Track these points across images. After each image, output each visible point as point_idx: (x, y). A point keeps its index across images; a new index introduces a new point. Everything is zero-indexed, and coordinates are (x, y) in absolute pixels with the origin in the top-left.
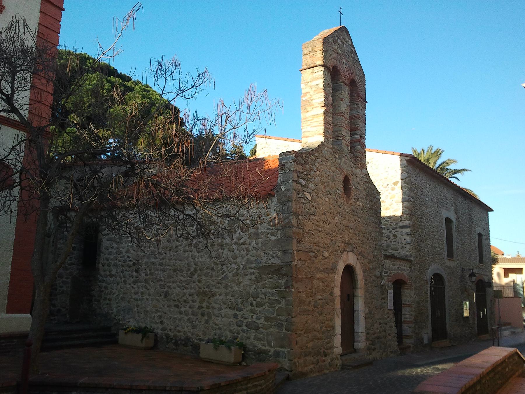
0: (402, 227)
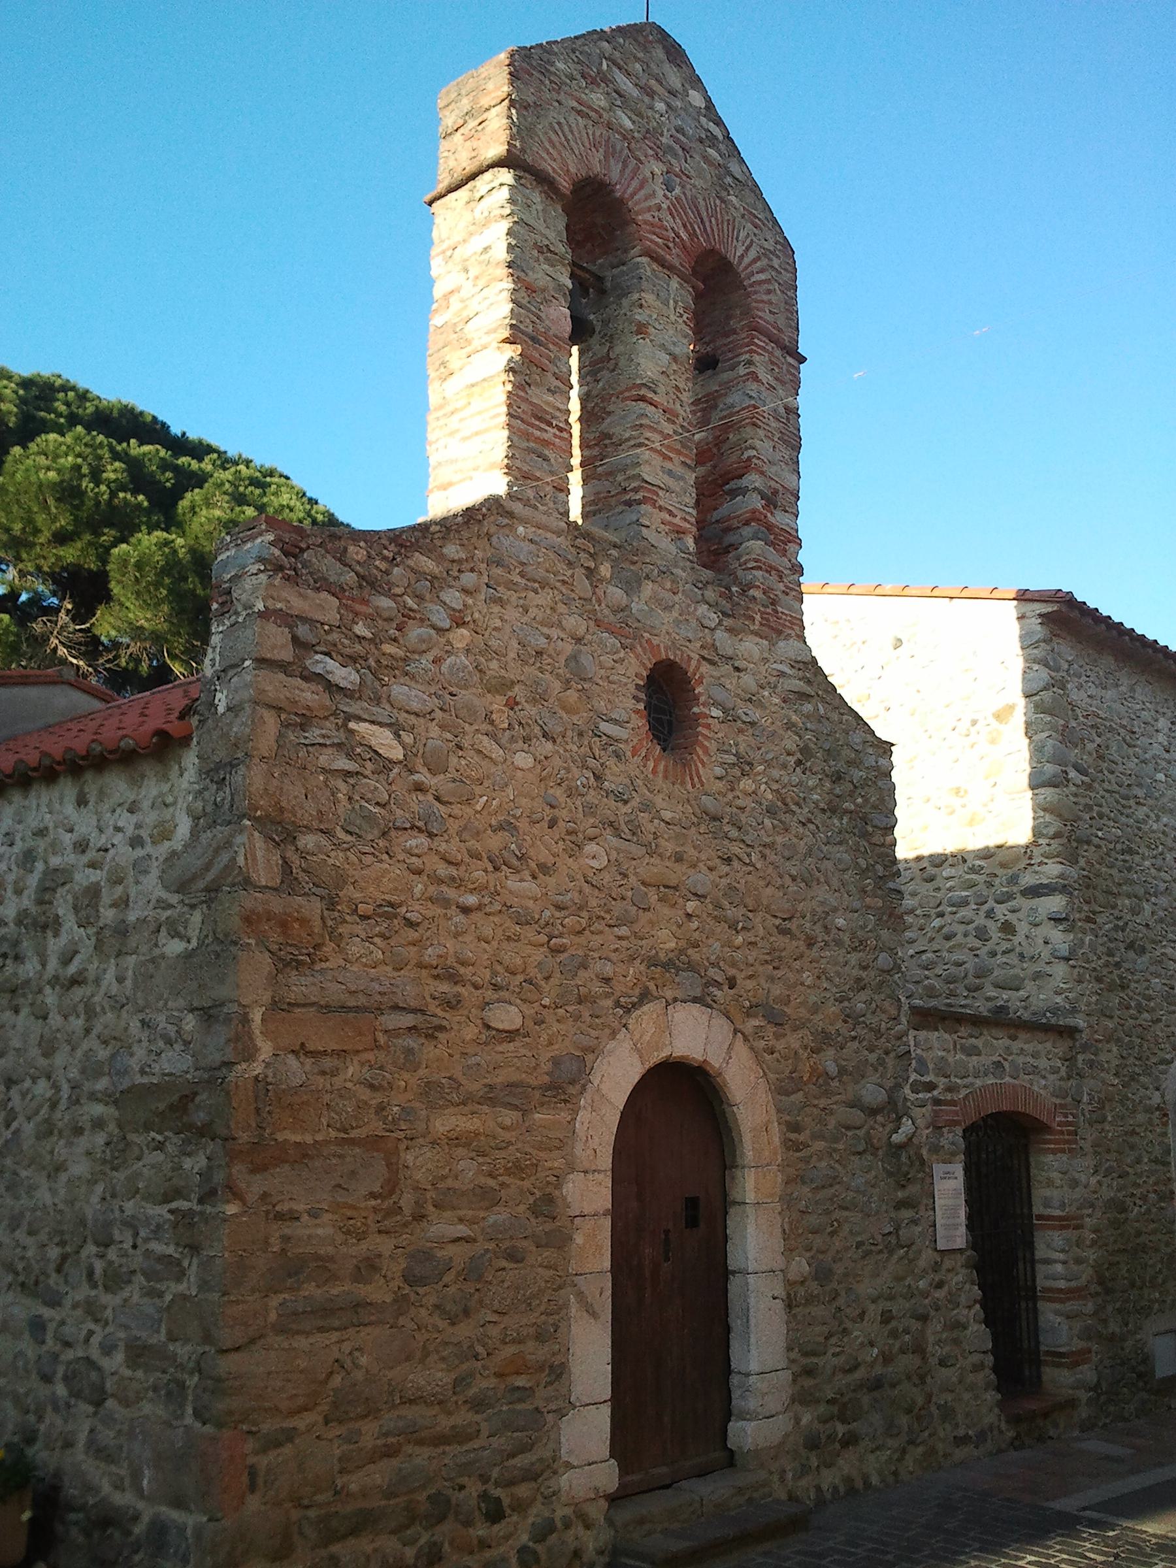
0: (1035, 892)
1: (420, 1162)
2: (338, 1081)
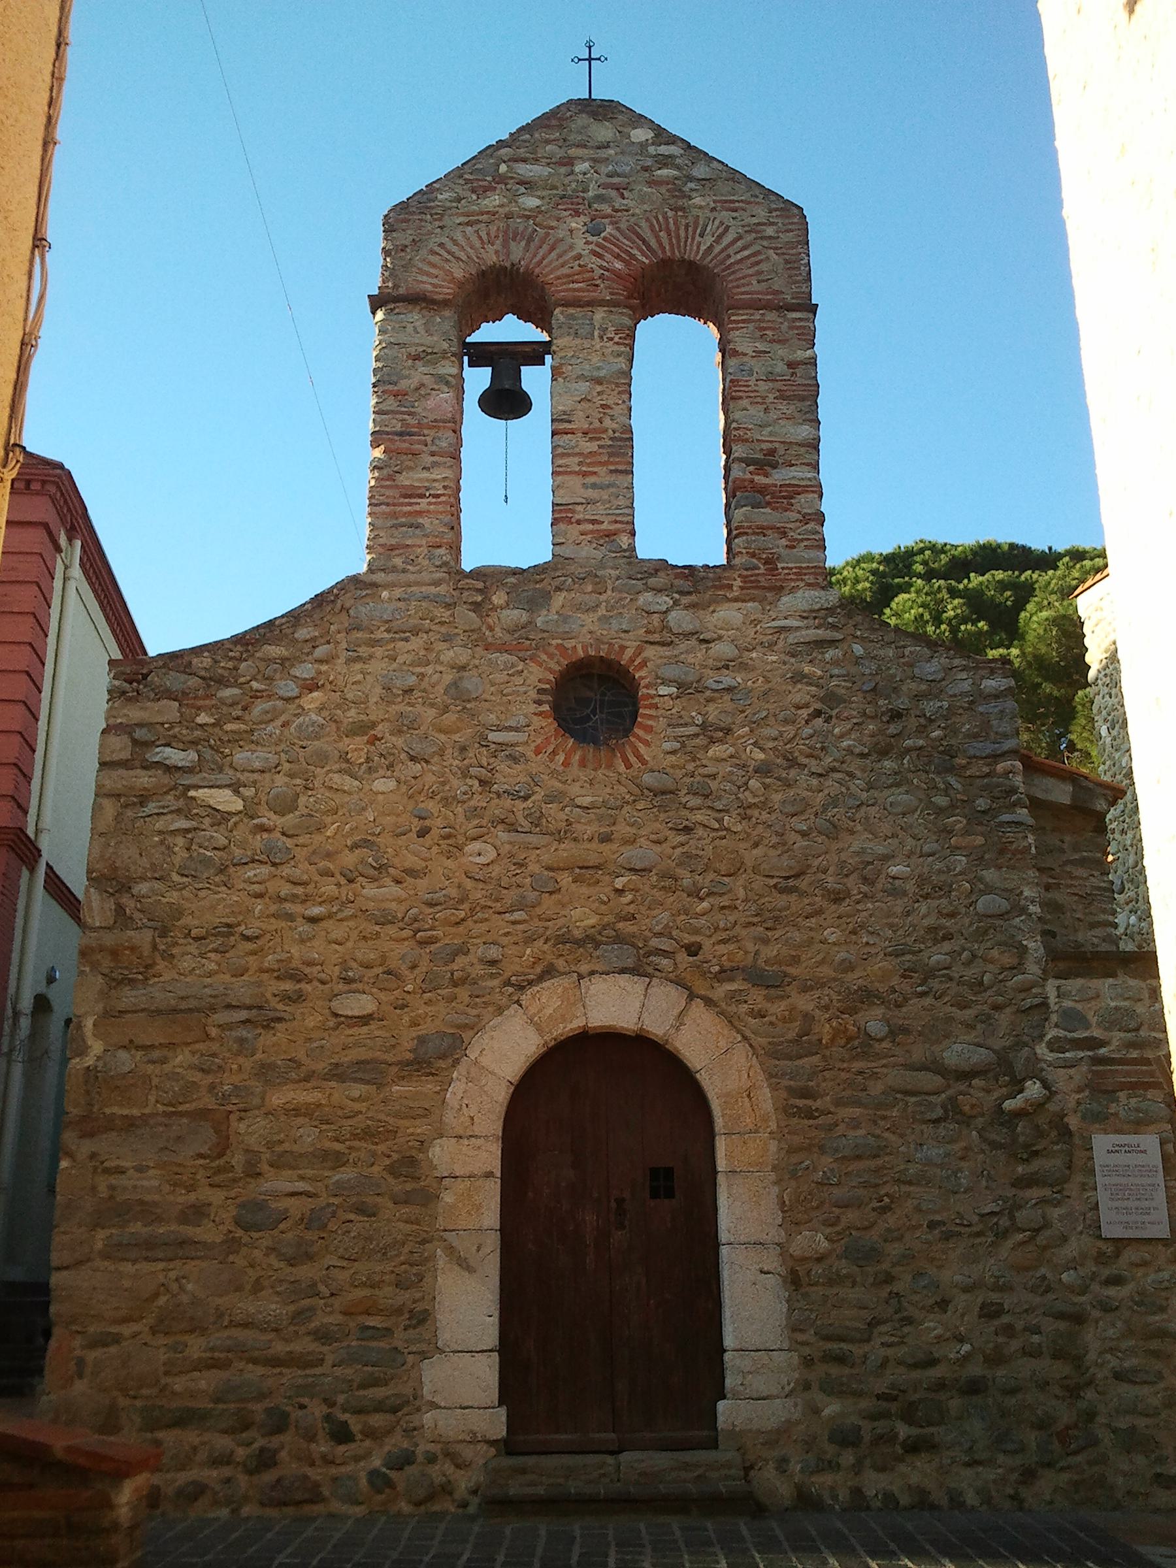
1: (251, 1131)
2: (167, 1068)
